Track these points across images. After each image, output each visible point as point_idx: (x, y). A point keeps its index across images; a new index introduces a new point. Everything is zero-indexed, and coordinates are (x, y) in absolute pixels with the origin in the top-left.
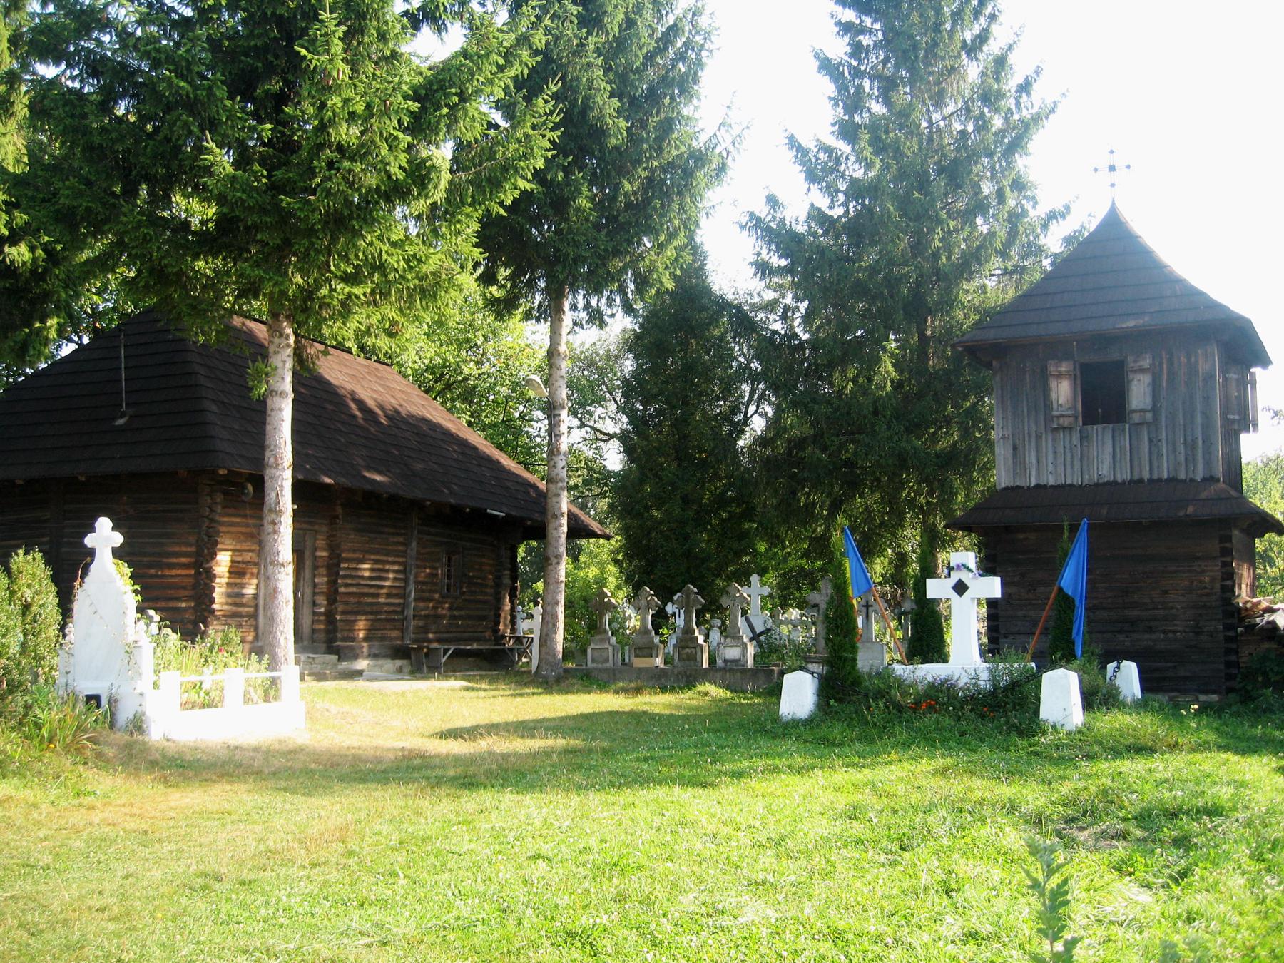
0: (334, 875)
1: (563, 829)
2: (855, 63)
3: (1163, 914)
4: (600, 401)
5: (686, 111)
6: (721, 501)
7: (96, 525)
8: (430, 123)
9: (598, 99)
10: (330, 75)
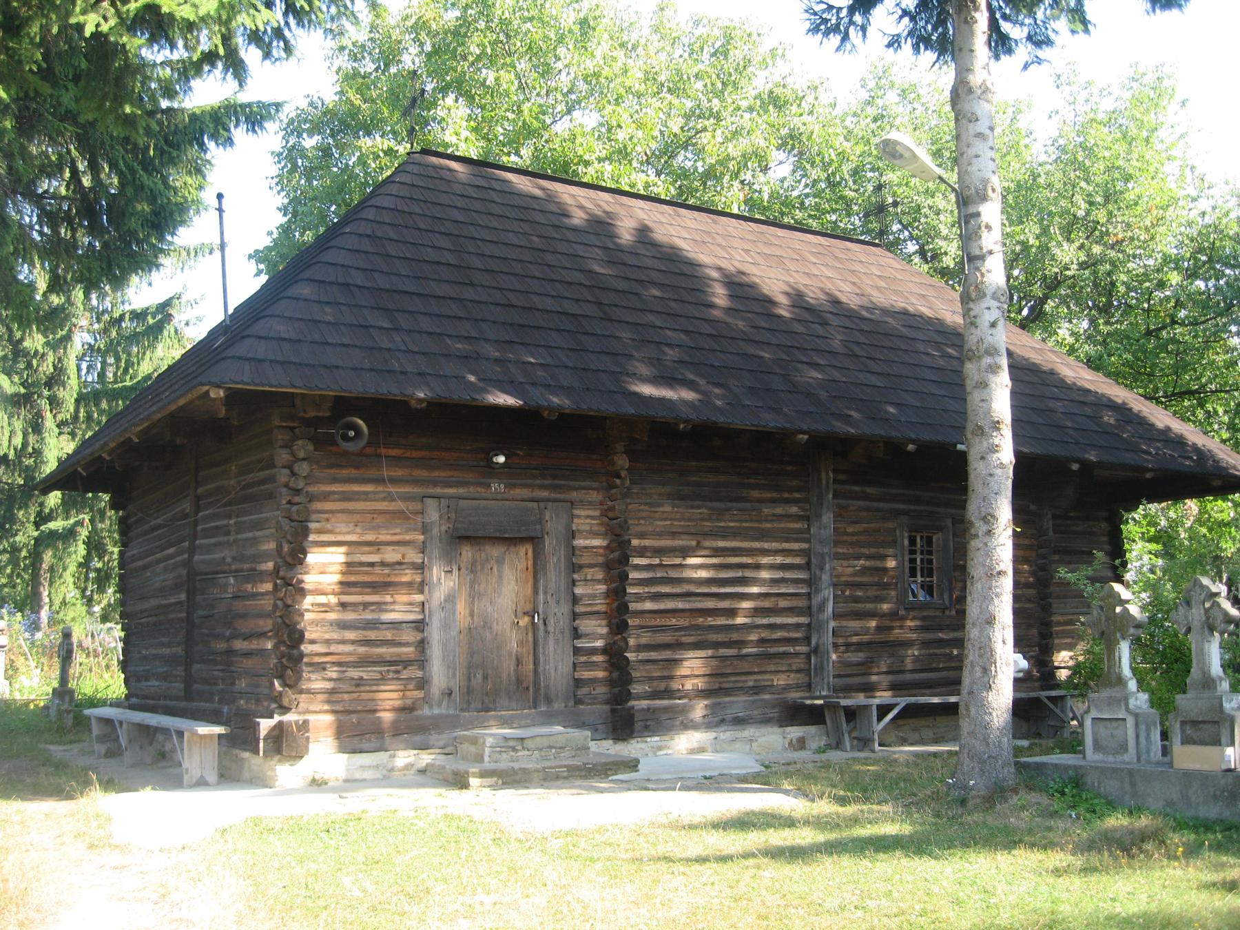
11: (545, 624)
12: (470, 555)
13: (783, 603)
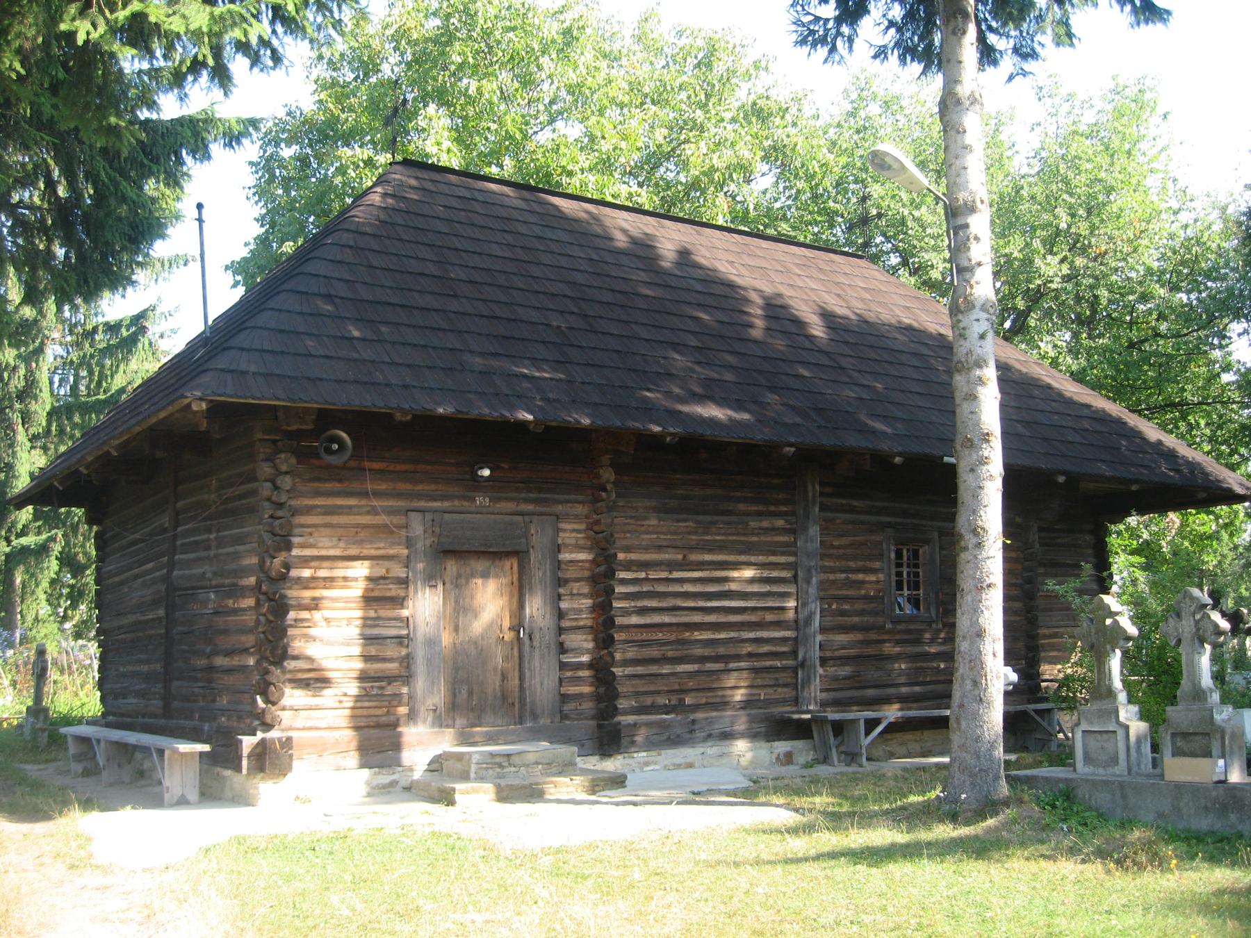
11: (531, 639)
12: (455, 569)
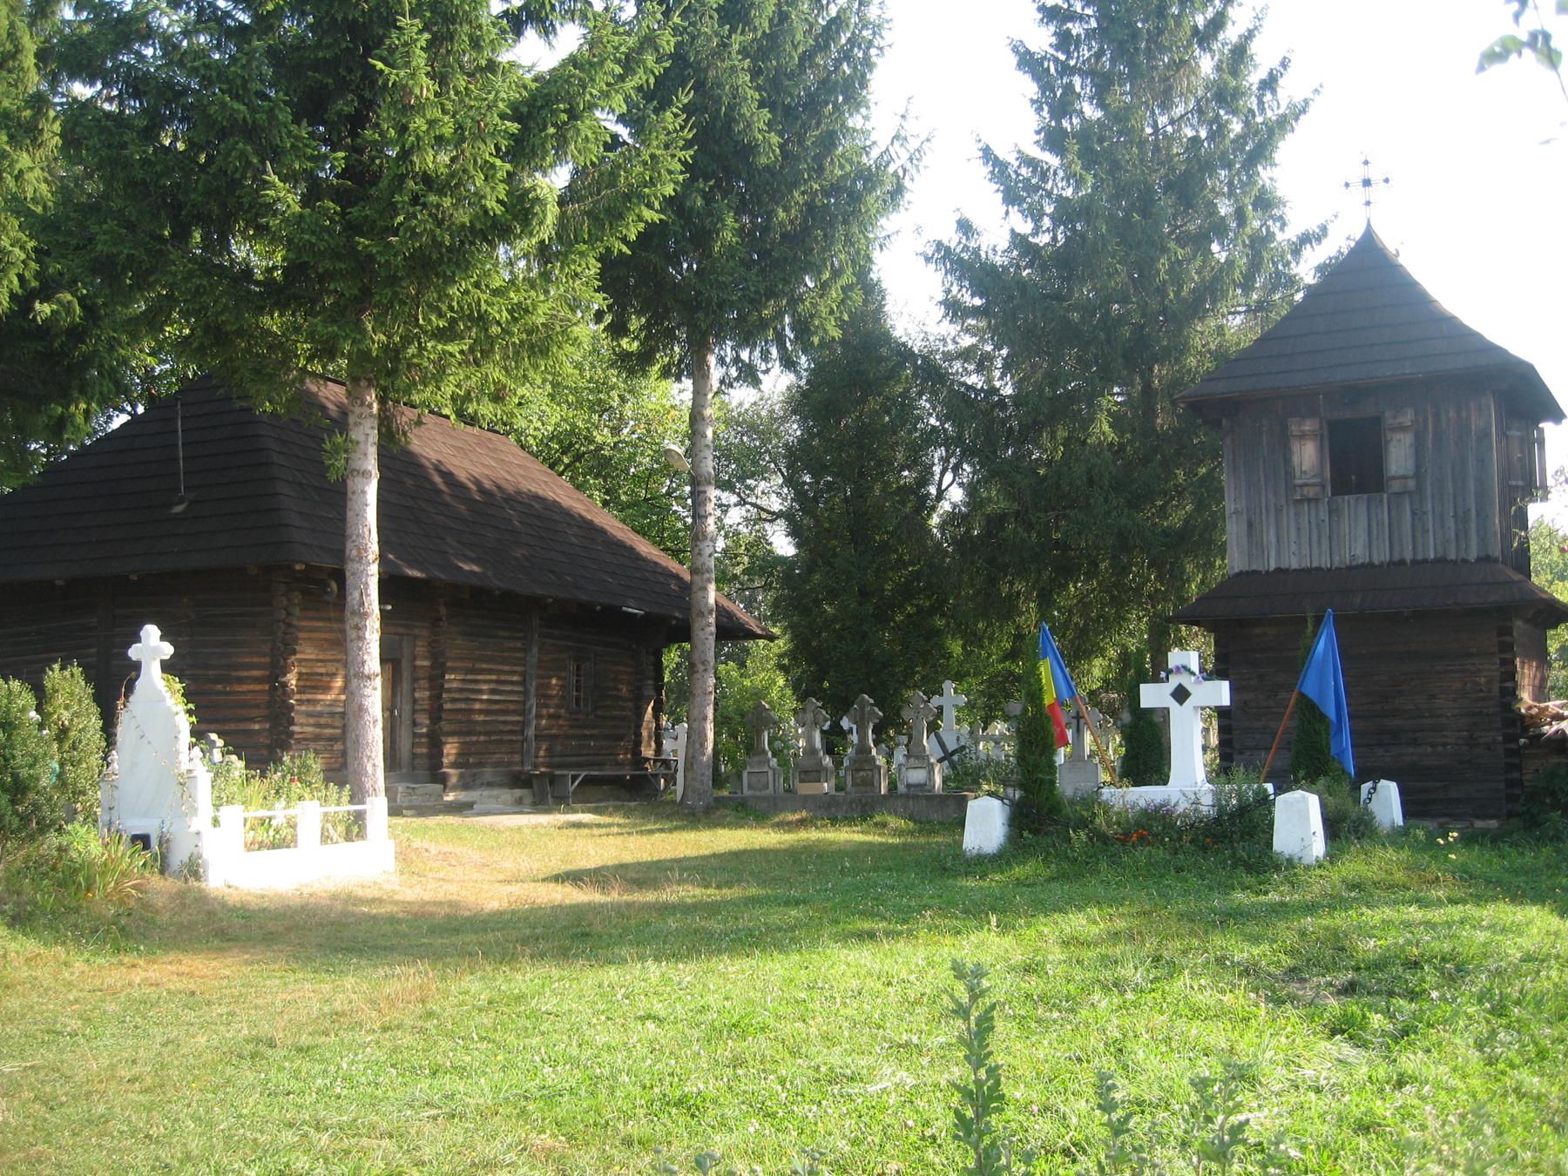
0: (407, 1040)
1: (684, 986)
2: (1062, 57)
3: (1370, 1077)
4: (761, 473)
5: (855, 121)
6: (906, 592)
7: (142, 633)
8: (534, 145)
9: (744, 110)
10: (411, 93)
13: (512, 707)
